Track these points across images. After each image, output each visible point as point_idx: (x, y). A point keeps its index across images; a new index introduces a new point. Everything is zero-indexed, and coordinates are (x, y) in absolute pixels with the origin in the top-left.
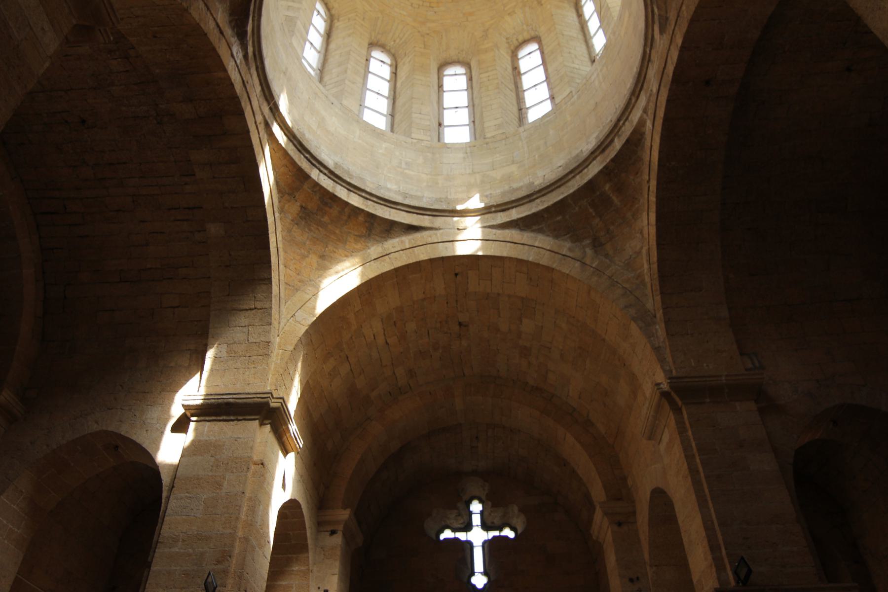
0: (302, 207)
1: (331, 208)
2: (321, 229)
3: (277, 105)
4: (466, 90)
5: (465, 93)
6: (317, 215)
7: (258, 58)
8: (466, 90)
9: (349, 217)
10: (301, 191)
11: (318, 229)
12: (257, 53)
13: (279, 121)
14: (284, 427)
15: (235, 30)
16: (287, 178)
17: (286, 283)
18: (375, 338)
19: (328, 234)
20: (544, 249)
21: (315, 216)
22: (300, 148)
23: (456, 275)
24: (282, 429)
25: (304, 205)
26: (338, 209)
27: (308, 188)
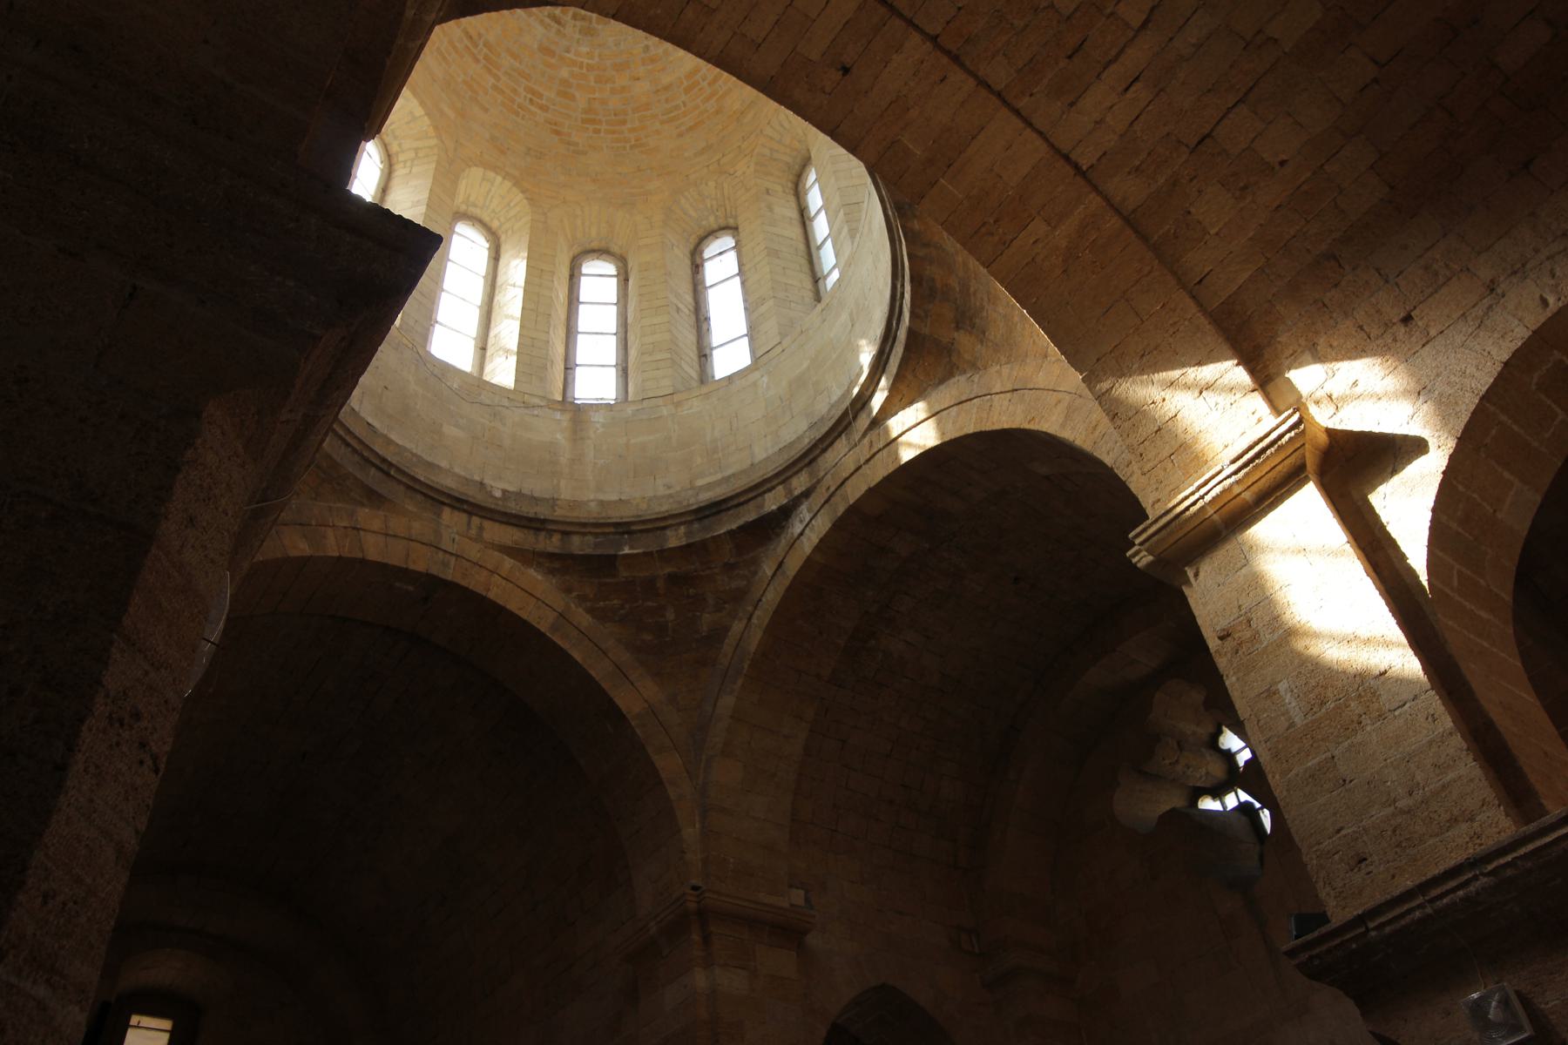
0: (957, 328)
1: (933, 280)
2: (972, 289)
3: (876, 359)
4: (615, 304)
5: (615, 308)
6: (956, 299)
7: (811, 457)
8: (615, 304)
9: (927, 245)
10: (936, 336)
11: (975, 294)
12: (807, 460)
13: (871, 390)
14: (1211, 511)
15: (784, 523)
16: (929, 365)
17: (1029, 422)
18: (1136, 79)
19: (973, 276)
20: (526, 592)
21: (958, 302)
22: (891, 340)
23: (846, 71)
24: (1216, 517)
25: (953, 325)
26: (928, 267)
27: (926, 326)
